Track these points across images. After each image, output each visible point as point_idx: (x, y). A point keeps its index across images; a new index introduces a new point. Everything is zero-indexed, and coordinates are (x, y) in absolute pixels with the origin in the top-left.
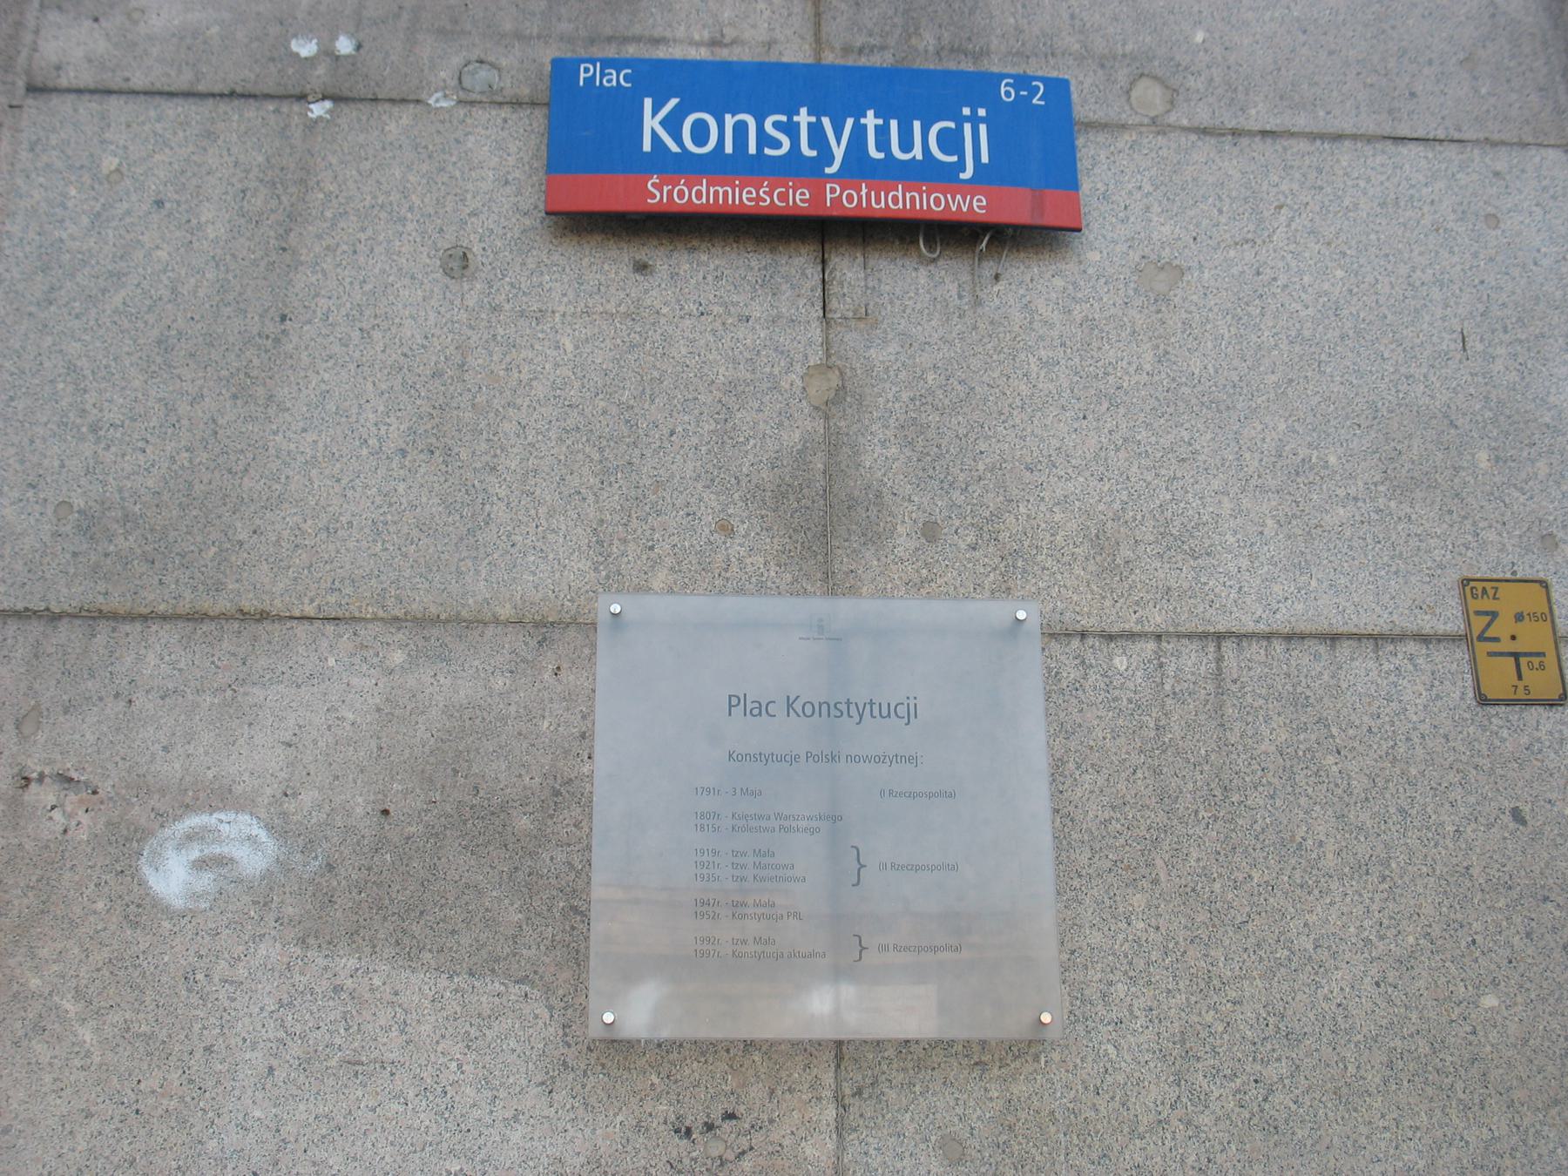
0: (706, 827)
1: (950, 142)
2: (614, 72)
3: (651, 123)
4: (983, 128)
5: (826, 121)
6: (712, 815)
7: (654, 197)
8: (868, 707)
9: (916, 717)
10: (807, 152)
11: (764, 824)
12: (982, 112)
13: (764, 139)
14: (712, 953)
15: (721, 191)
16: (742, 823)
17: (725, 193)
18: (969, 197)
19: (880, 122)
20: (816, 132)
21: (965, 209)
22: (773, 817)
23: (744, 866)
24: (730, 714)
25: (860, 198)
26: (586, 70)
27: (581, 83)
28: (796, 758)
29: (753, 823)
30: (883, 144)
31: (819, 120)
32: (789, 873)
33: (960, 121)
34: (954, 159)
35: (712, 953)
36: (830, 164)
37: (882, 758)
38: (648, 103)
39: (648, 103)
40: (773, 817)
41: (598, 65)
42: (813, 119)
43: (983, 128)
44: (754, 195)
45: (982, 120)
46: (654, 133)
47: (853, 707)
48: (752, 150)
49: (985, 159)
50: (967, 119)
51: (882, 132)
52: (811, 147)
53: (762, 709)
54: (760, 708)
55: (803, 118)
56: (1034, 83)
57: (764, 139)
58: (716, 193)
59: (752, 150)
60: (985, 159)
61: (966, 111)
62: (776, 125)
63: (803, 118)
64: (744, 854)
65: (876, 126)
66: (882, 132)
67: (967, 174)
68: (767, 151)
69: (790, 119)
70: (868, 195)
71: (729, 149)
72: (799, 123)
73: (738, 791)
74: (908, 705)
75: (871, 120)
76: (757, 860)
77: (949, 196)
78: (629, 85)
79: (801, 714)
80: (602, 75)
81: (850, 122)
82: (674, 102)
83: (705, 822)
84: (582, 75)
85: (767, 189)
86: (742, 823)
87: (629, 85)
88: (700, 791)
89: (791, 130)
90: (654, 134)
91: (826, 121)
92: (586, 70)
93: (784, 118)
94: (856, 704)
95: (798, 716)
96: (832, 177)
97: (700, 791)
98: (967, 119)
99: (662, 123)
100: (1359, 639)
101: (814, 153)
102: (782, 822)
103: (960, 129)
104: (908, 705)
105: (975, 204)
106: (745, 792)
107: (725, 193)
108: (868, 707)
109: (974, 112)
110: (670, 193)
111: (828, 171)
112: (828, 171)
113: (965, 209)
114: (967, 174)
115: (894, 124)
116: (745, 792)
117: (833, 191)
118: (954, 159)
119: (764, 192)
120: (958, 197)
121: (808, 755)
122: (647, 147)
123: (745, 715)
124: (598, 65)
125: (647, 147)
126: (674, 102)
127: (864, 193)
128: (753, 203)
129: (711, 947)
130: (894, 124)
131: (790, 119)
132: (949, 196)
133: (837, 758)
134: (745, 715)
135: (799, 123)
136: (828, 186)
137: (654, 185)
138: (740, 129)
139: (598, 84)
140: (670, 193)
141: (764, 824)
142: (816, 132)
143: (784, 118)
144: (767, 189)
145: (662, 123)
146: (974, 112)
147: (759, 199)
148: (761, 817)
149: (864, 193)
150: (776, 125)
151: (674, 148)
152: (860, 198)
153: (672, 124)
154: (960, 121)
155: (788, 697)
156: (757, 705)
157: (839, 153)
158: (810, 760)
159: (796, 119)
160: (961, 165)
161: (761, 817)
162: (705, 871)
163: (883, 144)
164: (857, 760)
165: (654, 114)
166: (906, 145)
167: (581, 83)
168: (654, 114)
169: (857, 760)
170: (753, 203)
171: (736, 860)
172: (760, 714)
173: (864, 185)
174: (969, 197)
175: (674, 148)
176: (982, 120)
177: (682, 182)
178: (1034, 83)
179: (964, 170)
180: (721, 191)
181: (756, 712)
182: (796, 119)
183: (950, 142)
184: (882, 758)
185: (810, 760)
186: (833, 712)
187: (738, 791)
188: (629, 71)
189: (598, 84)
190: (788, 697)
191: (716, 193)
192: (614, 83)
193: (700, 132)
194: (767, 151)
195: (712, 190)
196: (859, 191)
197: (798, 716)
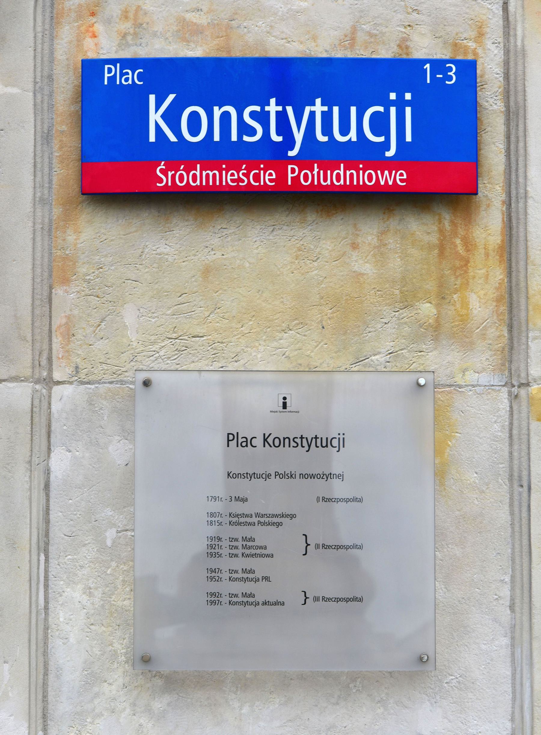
0: (213, 523)
2: (130, 72)
4: (408, 110)
5: (290, 110)
6: (218, 514)
7: (161, 181)
8: (314, 440)
9: (344, 447)
10: (276, 138)
11: (249, 520)
12: (408, 96)
13: (244, 129)
14: (217, 602)
15: (211, 174)
16: (235, 520)
17: (214, 176)
18: (394, 172)
19: (325, 109)
20: (282, 117)
21: (390, 183)
22: (254, 516)
23: (236, 547)
24: (228, 446)
25: (313, 176)
26: (110, 71)
28: (269, 476)
29: (242, 520)
30: (327, 129)
31: (285, 110)
32: (263, 552)
34: (382, 139)
35: (217, 602)
36: (292, 149)
37: (322, 476)
38: (152, 98)
39: (152, 98)
40: (254, 516)
41: (118, 65)
42: (280, 108)
43: (408, 110)
44: (236, 177)
45: (408, 103)
46: (157, 125)
47: (304, 441)
48: (234, 138)
49: (409, 138)
51: (327, 117)
52: (278, 134)
53: (248, 442)
54: (247, 441)
55: (273, 108)
56: (447, 65)
57: (244, 129)
58: (207, 176)
59: (234, 138)
60: (409, 138)
61: (393, 96)
62: (253, 115)
63: (273, 108)
64: (236, 540)
66: (327, 117)
67: (391, 153)
68: (246, 138)
69: (263, 109)
70: (319, 173)
71: (217, 137)
72: (269, 112)
73: (233, 499)
74: (339, 438)
75: (319, 108)
76: (244, 543)
77: (379, 172)
78: (142, 83)
79: (272, 445)
80: (122, 75)
82: (171, 97)
83: (213, 519)
85: (245, 171)
86: (235, 520)
87: (142, 83)
88: (210, 498)
90: (157, 125)
91: (290, 110)
92: (110, 71)
93: (257, 108)
94: (307, 438)
95: (271, 446)
96: (292, 160)
97: (210, 498)
99: (163, 116)
101: (280, 139)
102: (260, 519)
103: (387, 111)
104: (339, 438)
105: (398, 178)
106: (238, 499)
107: (214, 176)
108: (314, 440)
109: (400, 96)
110: (173, 176)
111: (291, 154)
112: (291, 154)
113: (390, 183)
115: (336, 110)
116: (238, 499)
117: (293, 171)
118: (382, 139)
119: (243, 174)
120: (386, 172)
121: (277, 474)
122: (152, 138)
123: (237, 446)
124: (118, 65)
125: (152, 138)
126: (171, 97)
127: (315, 172)
128: (235, 184)
129: (216, 599)
130: (336, 110)
131: (263, 109)
132: (379, 172)
133: (294, 476)
134: (237, 446)
135: (269, 112)
136: (290, 167)
137: (161, 171)
138: (225, 118)
139: (118, 83)
140: (173, 176)
141: (249, 520)
142: (282, 117)
143: (257, 108)
144: (245, 171)
145: (163, 116)
146: (400, 96)
147: (240, 180)
148: (247, 516)
149: (315, 172)
150: (253, 115)
151: (173, 138)
152: (313, 176)
154: (387, 104)
155: (264, 434)
156: (245, 440)
157: (299, 137)
158: (278, 477)
159: (267, 108)
160: (386, 145)
161: (247, 516)
162: (213, 551)
164: (306, 477)
165: (157, 109)
166: (345, 130)
168: (157, 109)
169: (306, 477)
170: (235, 184)
171: (232, 544)
172: (247, 446)
173: (316, 165)
174: (394, 172)
175: (173, 138)
176: (408, 103)
177: (182, 167)
178: (447, 65)
179: (389, 150)
180: (211, 174)
181: (244, 444)
182: (267, 108)
184: (322, 476)
185: (278, 477)
186: (293, 444)
187: (233, 499)
188: (142, 70)
189: (118, 83)
190: (264, 434)
191: (207, 176)
192: (130, 82)
194: (246, 138)
195: (204, 173)
196: (312, 170)
197: (271, 446)
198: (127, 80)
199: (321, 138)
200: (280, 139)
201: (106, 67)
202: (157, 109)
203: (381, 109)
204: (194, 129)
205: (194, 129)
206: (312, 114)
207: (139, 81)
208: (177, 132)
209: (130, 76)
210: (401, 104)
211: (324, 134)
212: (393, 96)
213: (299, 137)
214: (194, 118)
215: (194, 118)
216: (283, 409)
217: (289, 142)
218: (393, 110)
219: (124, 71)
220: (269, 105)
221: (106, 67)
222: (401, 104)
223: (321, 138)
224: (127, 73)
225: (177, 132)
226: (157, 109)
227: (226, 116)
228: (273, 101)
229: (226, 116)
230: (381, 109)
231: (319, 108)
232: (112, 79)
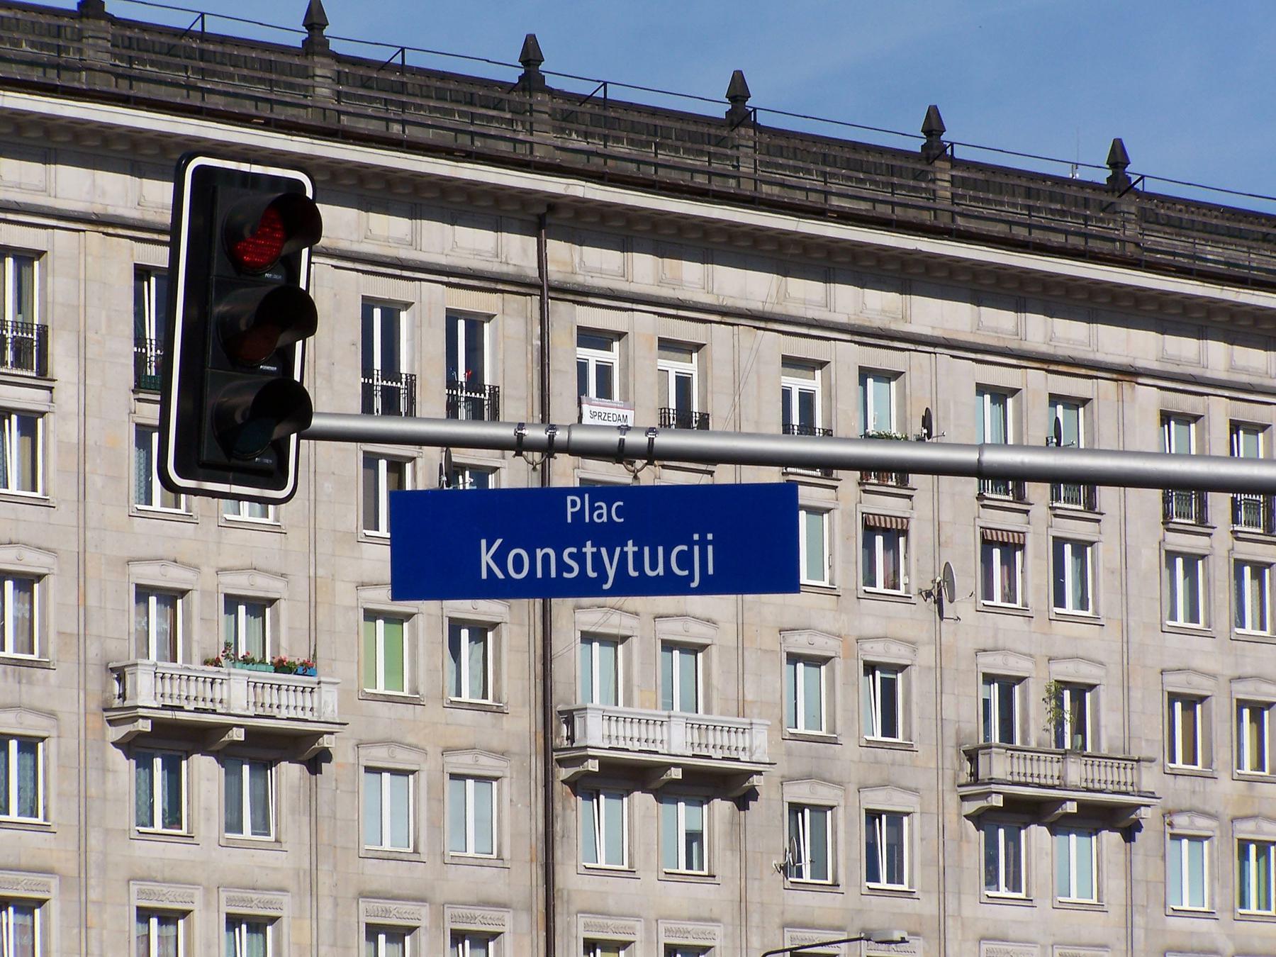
1: (685, 560)
3: (486, 558)
4: (710, 548)
5: (604, 551)
12: (710, 537)
20: (597, 558)
26: (574, 504)
27: (569, 520)
30: (639, 565)
33: (691, 544)
34: (686, 573)
36: (606, 583)
38: (484, 542)
39: (484, 542)
41: (587, 496)
43: (710, 548)
45: (710, 542)
46: (488, 565)
48: (553, 574)
49: (711, 571)
50: (696, 543)
51: (638, 557)
52: (594, 570)
59: (553, 574)
60: (711, 571)
62: (571, 555)
63: (589, 549)
65: (592, 553)
66: (638, 557)
67: (695, 584)
68: (566, 575)
72: (585, 553)
75: (630, 548)
78: (622, 520)
80: (592, 510)
81: (618, 550)
82: (499, 541)
84: (570, 510)
87: (622, 520)
89: (579, 558)
90: (488, 565)
91: (604, 551)
92: (574, 504)
93: (574, 550)
98: (696, 543)
100: (1139, 791)
101: (594, 575)
103: (691, 550)
109: (703, 537)
114: (695, 584)
115: (646, 550)
118: (686, 573)
122: (484, 576)
124: (587, 496)
125: (484, 576)
126: (499, 541)
130: (646, 550)
131: (579, 550)
135: (585, 553)
139: (587, 520)
142: (597, 558)
146: (703, 537)
150: (571, 555)
151: (501, 576)
153: (500, 558)
154: (691, 544)
157: (611, 573)
159: (584, 550)
160: (691, 577)
163: (639, 565)
166: (654, 566)
167: (569, 520)
175: (501, 576)
176: (710, 542)
182: (584, 550)
183: (685, 560)
188: (621, 503)
189: (587, 520)
192: (605, 519)
193: (518, 566)
198: (600, 516)
199: (633, 573)
200: (594, 575)
201: (569, 498)
202: (488, 551)
203: (685, 548)
204: (518, 568)
205: (518, 568)
206: (624, 555)
207: (618, 516)
208: (504, 568)
209: (605, 511)
210: (703, 544)
211: (635, 570)
212: (696, 537)
213: (611, 573)
214: (518, 558)
215: (518, 558)
216: (687, 868)
217: (603, 577)
218: (696, 548)
219: (596, 505)
220: (627, 546)
221: (569, 498)
222: (703, 544)
223: (633, 573)
224: (600, 507)
225: (504, 568)
226: (488, 551)
227: (546, 558)
228: (630, 543)
229: (546, 558)
230: (685, 548)
231: (630, 548)
232: (578, 515)
